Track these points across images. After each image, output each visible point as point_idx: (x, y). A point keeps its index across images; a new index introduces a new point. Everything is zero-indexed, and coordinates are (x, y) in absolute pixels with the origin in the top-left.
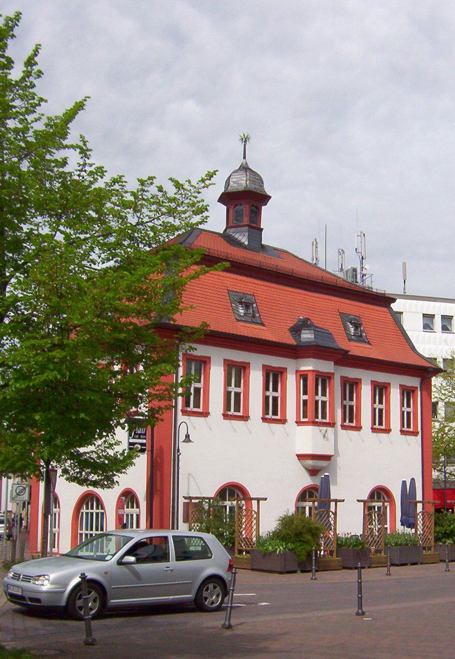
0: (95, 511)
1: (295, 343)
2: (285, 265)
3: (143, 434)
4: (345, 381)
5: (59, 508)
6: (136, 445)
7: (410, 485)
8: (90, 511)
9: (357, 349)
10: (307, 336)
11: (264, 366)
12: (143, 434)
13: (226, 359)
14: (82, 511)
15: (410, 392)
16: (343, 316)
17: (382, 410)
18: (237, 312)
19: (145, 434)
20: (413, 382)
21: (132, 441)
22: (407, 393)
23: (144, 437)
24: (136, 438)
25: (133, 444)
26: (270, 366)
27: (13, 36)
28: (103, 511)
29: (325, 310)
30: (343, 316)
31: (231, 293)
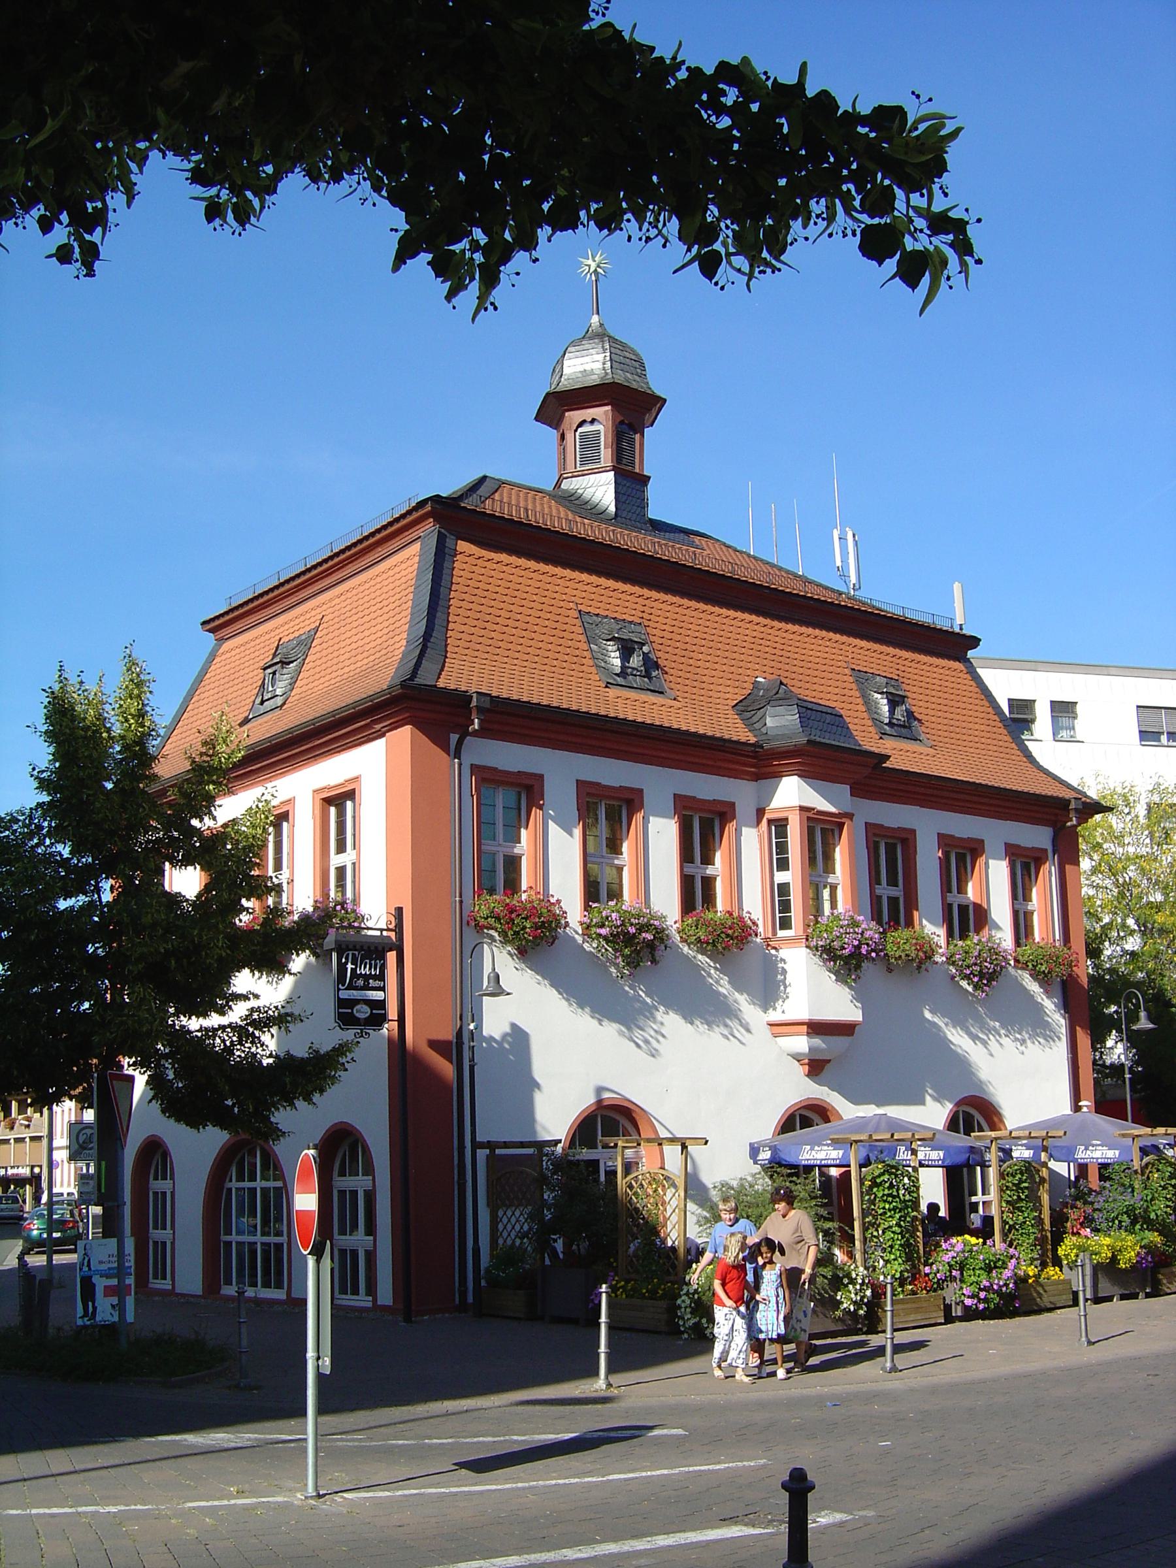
0: (259, 1184)
1: (753, 740)
2: (707, 559)
3: (375, 977)
4: (874, 833)
5: (172, 1178)
6: (358, 1007)
7: (686, 1182)
8: (247, 1184)
9: (904, 756)
10: (780, 722)
11: (677, 798)
12: (375, 977)
13: (477, 767)
14: (228, 1185)
15: (712, 820)
16: (862, 678)
17: (897, 899)
18: (603, 664)
19: (381, 977)
20: (1037, 836)
21: (344, 994)
22: (1025, 865)
23: (377, 983)
24: (356, 988)
25: (352, 1003)
26: (598, 784)
27: (405, 252)
28: (279, 1184)
29: (825, 665)
30: (862, 678)
31: (586, 618)
